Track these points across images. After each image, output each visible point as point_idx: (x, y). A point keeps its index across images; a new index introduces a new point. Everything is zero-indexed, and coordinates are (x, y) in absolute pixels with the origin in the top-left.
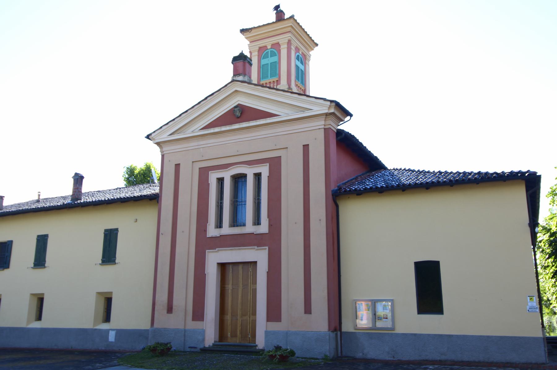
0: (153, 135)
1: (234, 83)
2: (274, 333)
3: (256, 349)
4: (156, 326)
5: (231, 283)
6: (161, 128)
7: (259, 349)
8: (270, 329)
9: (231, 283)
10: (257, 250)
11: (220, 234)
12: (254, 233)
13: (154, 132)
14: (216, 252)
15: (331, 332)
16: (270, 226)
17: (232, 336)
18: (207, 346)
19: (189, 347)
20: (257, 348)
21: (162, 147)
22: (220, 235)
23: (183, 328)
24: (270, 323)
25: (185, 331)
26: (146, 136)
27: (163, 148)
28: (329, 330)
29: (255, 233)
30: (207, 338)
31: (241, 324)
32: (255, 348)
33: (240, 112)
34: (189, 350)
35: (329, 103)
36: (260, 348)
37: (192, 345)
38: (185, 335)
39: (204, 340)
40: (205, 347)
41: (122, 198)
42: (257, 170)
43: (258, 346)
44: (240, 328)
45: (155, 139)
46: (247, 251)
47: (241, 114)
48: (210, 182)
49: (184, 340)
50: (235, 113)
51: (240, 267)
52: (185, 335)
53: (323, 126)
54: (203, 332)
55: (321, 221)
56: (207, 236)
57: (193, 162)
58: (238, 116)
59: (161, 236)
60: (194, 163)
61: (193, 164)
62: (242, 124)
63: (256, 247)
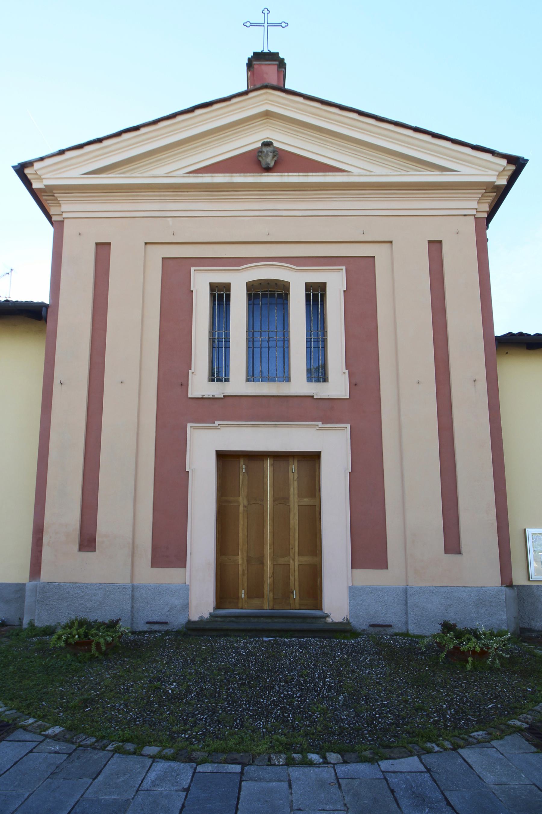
0: (37, 165)
1: (267, 93)
2: (372, 590)
3: (326, 623)
4: (45, 576)
5: (243, 492)
6: (62, 152)
7: (333, 623)
8: (358, 583)
9: (243, 492)
10: (321, 429)
11: (223, 393)
12: (313, 396)
13: (42, 159)
14: (216, 428)
15: (505, 587)
16: (353, 385)
17: (249, 596)
18: (194, 617)
19: (148, 623)
20: (329, 620)
21: (56, 199)
22: (224, 396)
23: (129, 582)
24: (358, 572)
25: (133, 588)
26: (16, 164)
27: (60, 206)
28: (502, 584)
29: (315, 397)
30: (194, 601)
31: (273, 573)
32: (324, 620)
33: (273, 157)
34: (146, 628)
35: (504, 162)
36: (336, 620)
37: (154, 619)
38: (133, 597)
39: (186, 607)
40: (189, 622)
41: (17, 165)
42: (316, 277)
43: (331, 616)
44: (271, 580)
45: (42, 177)
46: (294, 430)
47: (276, 162)
48: (194, 287)
49: (132, 607)
50: (260, 159)
51: (268, 463)
52: (133, 597)
53: (475, 211)
54: (185, 589)
55: (476, 382)
56: (190, 396)
57: (146, 243)
58: (269, 164)
59: (56, 389)
60: (148, 246)
61: (145, 248)
62: (288, 176)
63: (320, 424)
